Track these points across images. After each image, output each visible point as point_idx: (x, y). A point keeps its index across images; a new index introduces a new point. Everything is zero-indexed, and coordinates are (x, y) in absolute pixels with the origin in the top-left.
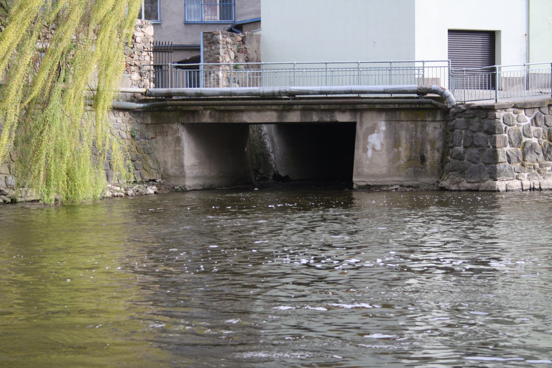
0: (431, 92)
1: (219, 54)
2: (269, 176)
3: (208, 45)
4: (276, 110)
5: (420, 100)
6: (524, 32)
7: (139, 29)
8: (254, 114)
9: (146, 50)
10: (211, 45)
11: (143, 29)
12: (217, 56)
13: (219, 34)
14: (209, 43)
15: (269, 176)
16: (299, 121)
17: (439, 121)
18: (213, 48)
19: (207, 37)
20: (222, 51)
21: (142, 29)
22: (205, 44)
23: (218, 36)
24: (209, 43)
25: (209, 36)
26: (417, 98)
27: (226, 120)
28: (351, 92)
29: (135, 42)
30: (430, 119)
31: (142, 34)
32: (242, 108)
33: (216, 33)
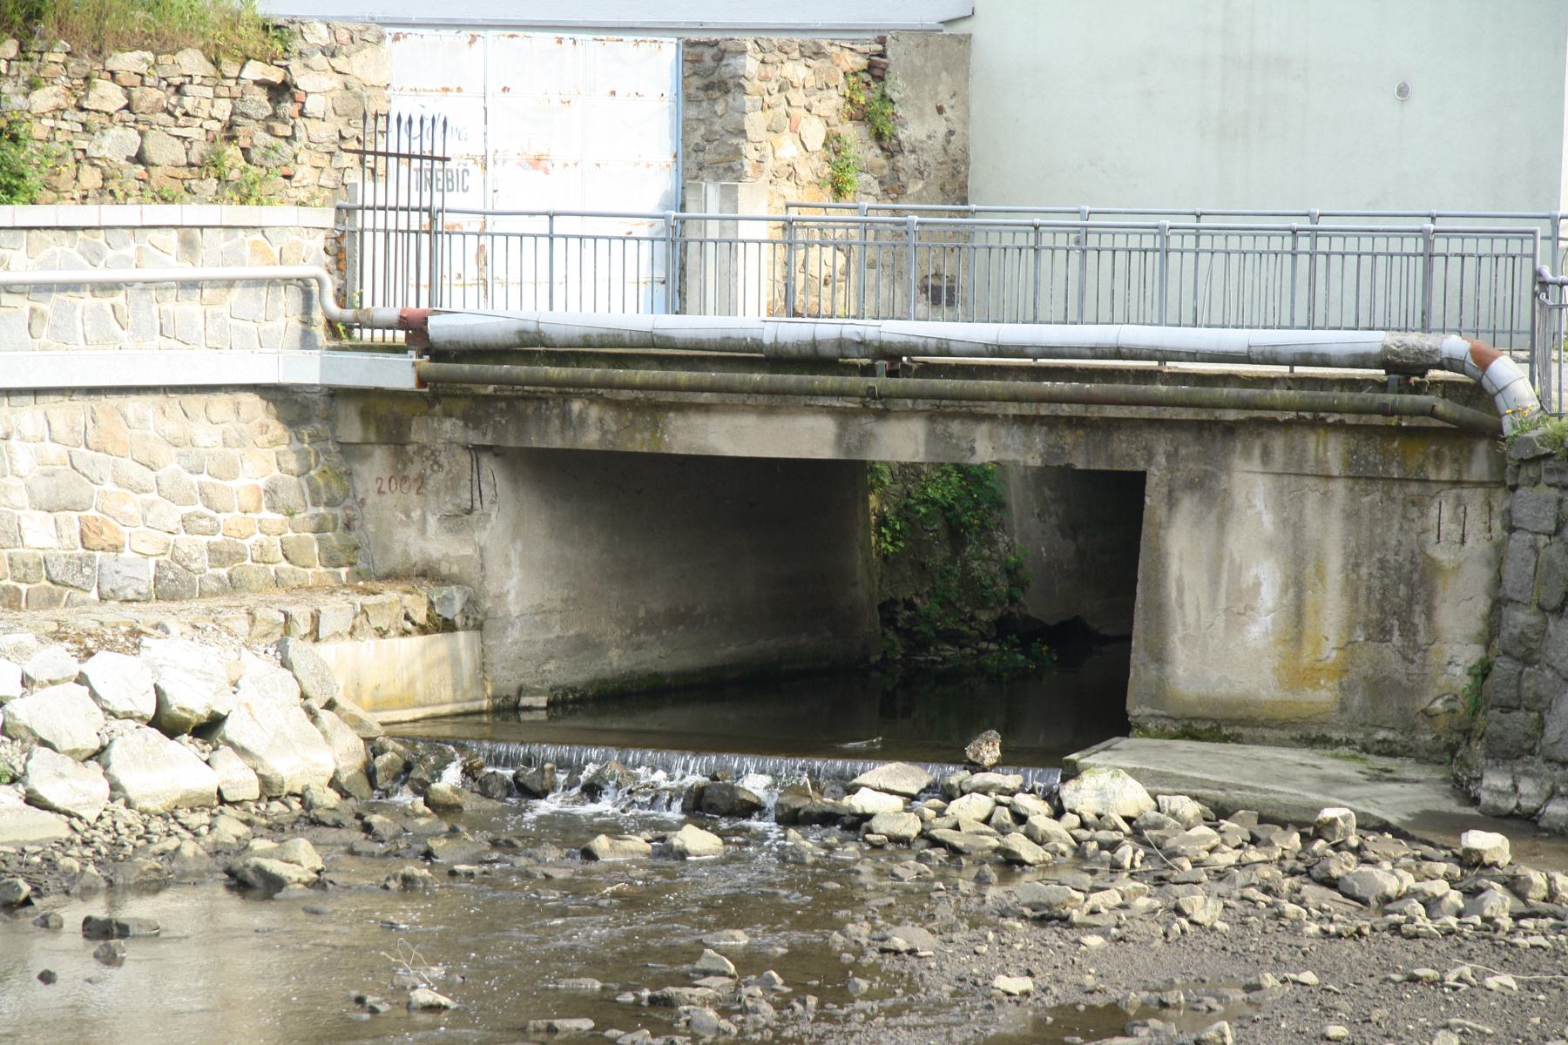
0: (1440, 366)
1: (742, 132)
2: (335, 518)
3: (701, 95)
4: (830, 411)
5: (1389, 398)
6: (29, 399)
7: (318, 60)
8: (749, 422)
9: (354, 145)
10: (716, 94)
11: (339, 63)
12: (735, 141)
13: (743, 52)
14: (708, 88)
15: (335, 518)
16: (826, 453)
17: (1480, 484)
18: (719, 108)
19: (697, 60)
20: (755, 123)
21: (334, 62)
22: (692, 91)
23: (740, 60)
24: (708, 88)
25: (708, 53)
26: (1382, 386)
27: (640, 443)
28: (1118, 353)
29: (302, 114)
30: (1446, 474)
31: (337, 81)
32: (705, 397)
33: (731, 46)
